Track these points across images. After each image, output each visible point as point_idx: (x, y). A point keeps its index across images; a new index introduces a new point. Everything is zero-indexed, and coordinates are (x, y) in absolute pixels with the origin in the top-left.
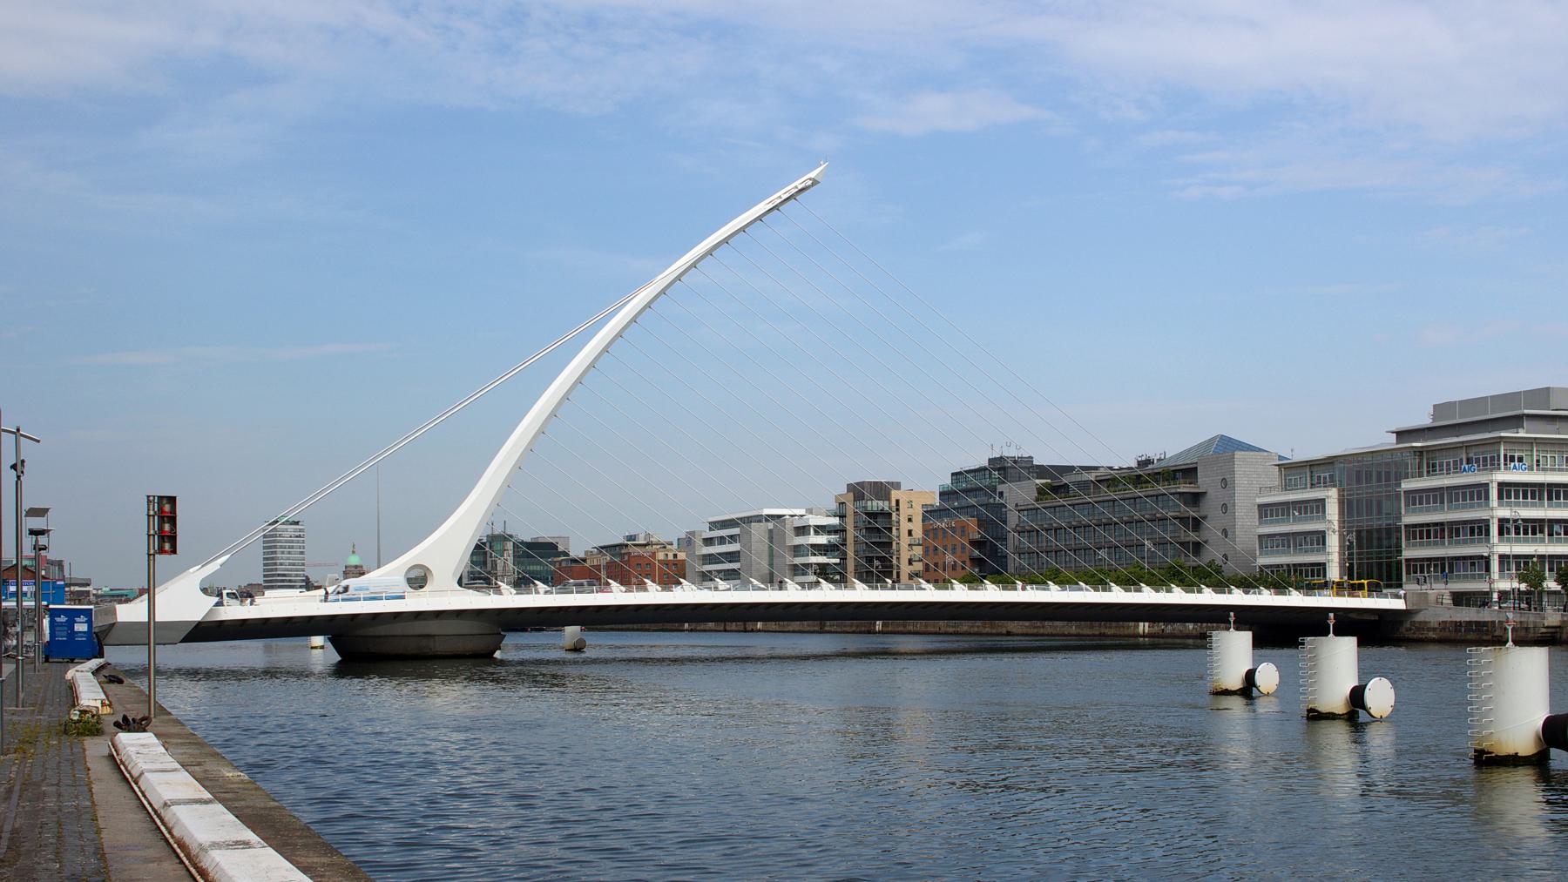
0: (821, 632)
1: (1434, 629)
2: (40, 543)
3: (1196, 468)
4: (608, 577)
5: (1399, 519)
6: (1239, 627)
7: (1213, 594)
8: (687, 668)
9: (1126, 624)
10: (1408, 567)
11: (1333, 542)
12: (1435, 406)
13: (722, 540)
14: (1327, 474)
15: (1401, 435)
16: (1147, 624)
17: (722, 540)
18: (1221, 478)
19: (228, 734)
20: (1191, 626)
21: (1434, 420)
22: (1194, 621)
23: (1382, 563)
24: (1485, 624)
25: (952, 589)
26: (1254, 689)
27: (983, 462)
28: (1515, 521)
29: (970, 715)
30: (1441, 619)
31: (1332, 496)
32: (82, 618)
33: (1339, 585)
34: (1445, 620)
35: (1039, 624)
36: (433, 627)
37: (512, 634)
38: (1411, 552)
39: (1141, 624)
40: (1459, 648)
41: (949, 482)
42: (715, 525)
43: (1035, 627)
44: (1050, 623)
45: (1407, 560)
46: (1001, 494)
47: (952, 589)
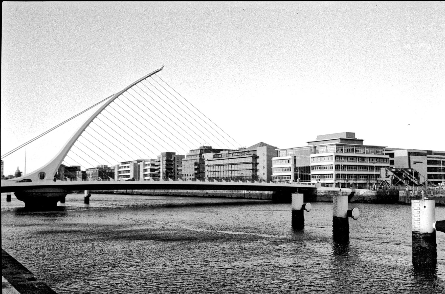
1: (323, 193)
2: (251, 161)
4: (99, 177)
5: (310, 164)
6: (300, 192)
9: (240, 191)
12: (317, 136)
13: (125, 167)
14: (372, 151)
16: (245, 191)
17: (125, 167)
18: (262, 153)
22: (172, 189)
23: (302, 176)
24: (336, 191)
25: (178, 181)
26: (304, 210)
28: (341, 165)
29: (189, 216)
30: (325, 190)
34: (325, 190)
36: (47, 190)
37: (93, 194)
38: (313, 172)
39: (244, 191)
41: (189, 153)
42: (123, 163)
45: (312, 175)
46: (203, 156)
47: (178, 181)
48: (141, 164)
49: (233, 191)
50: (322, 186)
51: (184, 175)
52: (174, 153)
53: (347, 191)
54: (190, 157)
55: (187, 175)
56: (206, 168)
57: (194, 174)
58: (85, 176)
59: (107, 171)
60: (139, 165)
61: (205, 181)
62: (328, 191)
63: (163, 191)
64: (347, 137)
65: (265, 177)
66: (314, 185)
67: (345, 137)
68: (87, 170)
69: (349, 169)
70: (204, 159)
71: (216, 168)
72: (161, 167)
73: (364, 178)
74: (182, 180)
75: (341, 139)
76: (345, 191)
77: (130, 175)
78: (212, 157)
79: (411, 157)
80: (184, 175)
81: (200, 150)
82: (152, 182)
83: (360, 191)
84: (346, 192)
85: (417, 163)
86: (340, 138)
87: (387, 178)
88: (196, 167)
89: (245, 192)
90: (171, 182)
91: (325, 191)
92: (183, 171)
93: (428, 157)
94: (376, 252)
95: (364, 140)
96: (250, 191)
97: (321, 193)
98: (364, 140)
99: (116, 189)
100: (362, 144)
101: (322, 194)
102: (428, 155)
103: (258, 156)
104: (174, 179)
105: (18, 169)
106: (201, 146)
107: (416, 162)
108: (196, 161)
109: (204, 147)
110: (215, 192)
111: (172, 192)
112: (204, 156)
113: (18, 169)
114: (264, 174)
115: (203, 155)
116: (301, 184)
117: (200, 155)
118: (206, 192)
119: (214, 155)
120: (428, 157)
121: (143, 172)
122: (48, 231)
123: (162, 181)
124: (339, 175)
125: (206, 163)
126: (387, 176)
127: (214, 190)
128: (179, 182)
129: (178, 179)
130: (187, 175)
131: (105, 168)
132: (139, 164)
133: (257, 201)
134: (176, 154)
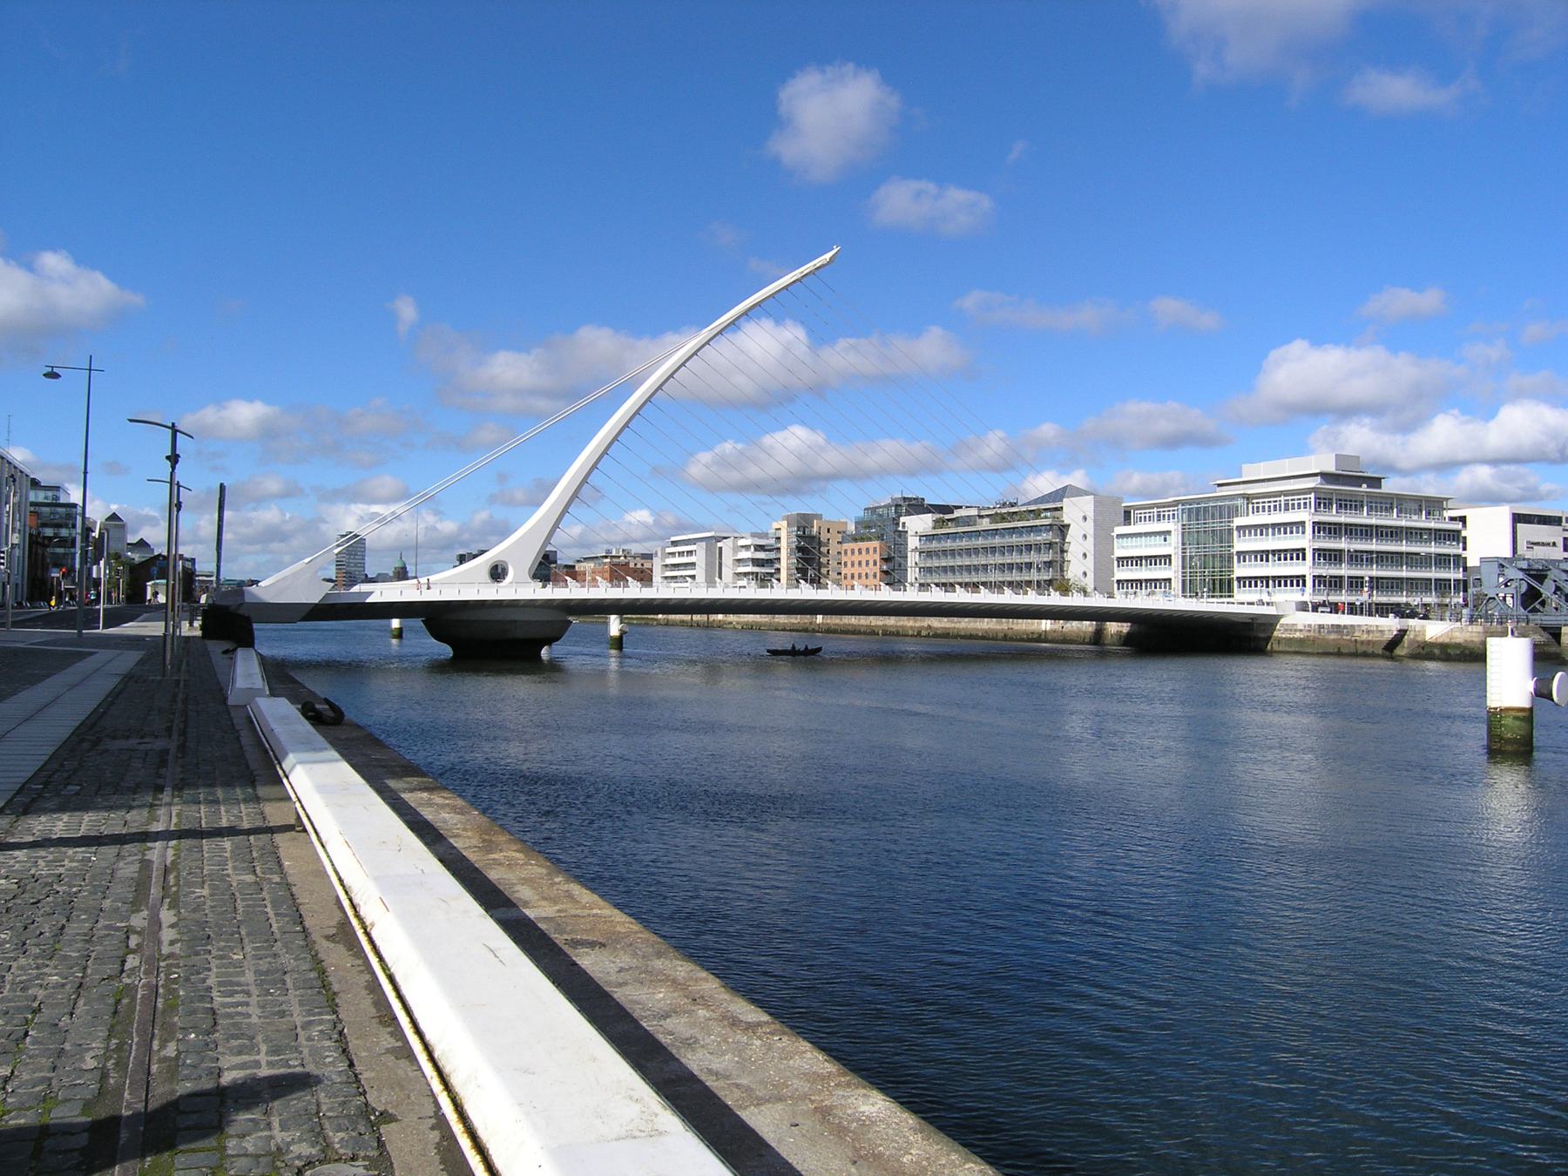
1: (1301, 630)
11: (1176, 562)
16: (1049, 621)
31: (1172, 526)
38: (1240, 570)
46: (904, 523)
50: (1298, 610)
52: (819, 517)
53: (1382, 626)
56: (1172, 547)
60: (721, 548)
61: (979, 592)
62: (1320, 625)
63: (796, 619)
64: (1337, 470)
65: (1089, 583)
66: (1274, 607)
68: (578, 561)
69: (1382, 561)
70: (907, 532)
72: (784, 555)
74: (1264, 601)
75: (1326, 476)
76: (1377, 626)
78: (931, 524)
82: (753, 592)
83: (1423, 627)
84: (1380, 629)
85: (1535, 547)
86: (1317, 471)
90: (806, 592)
91: (1310, 626)
97: (1296, 630)
99: (663, 614)
101: (1298, 635)
103: (1066, 522)
104: (816, 582)
107: (1533, 544)
112: (906, 524)
114: (1085, 574)
115: (902, 519)
116: (1228, 603)
118: (925, 624)
119: (936, 521)
121: (731, 567)
123: (779, 591)
124: (1447, 583)
129: (1048, 590)
131: (625, 557)
132: (719, 545)
133: (1045, 647)
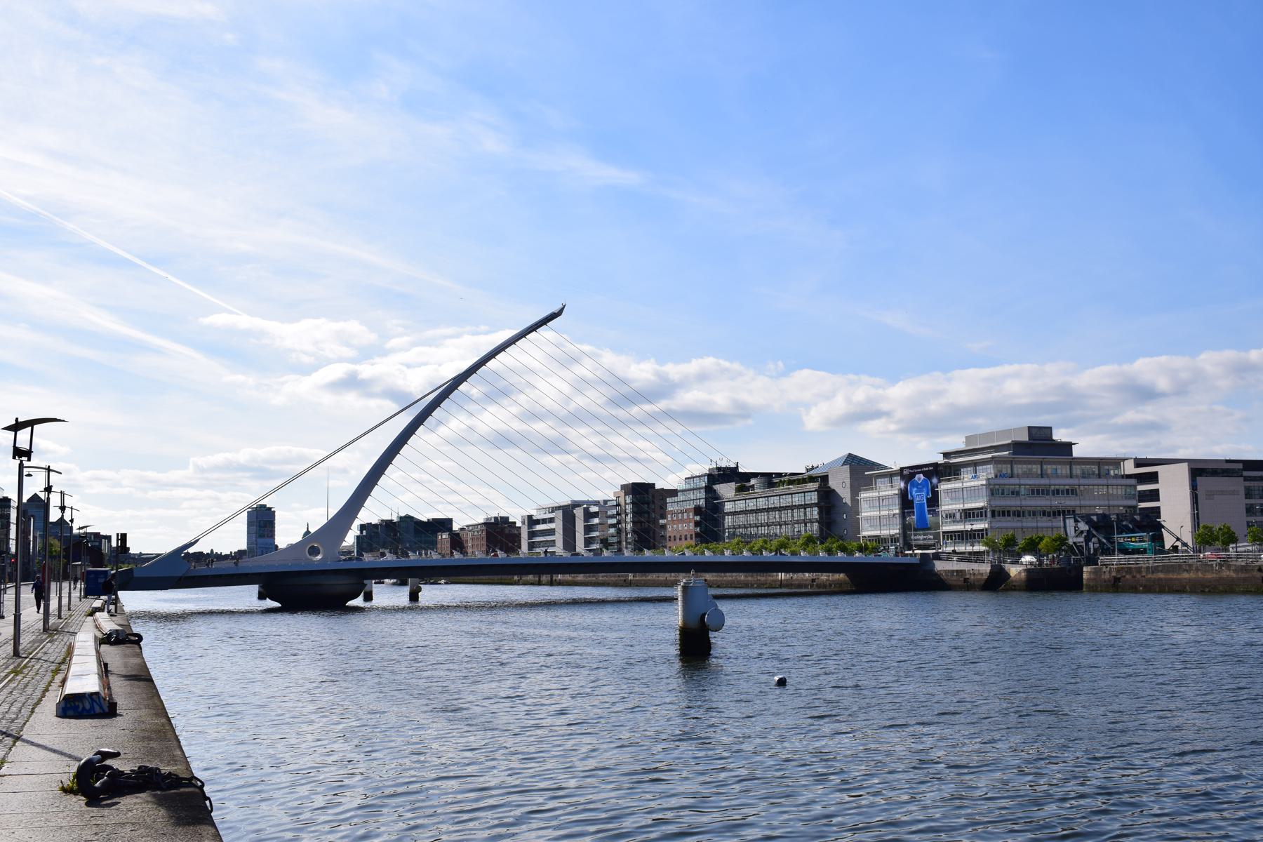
0: (539, 583)
3: (828, 476)
7: (387, 517)
8: (214, 618)
10: (944, 536)
15: (946, 455)
16: (783, 574)
19: (356, 645)
20: (807, 575)
21: (967, 445)
22: (786, 571)
24: (961, 571)
27: (320, 370)
32: (102, 576)
33: (1255, 592)
35: (723, 574)
39: (780, 574)
40: (924, 593)
43: (721, 577)
44: (730, 574)
48: (579, 513)
49: (746, 576)
51: (672, 539)
54: (686, 493)
55: (683, 539)
56: (728, 521)
57: (694, 536)
58: (457, 541)
59: (507, 531)
67: (1024, 437)
71: (812, 512)
73: (951, 539)
76: (979, 570)
77: (554, 541)
79: (1200, 480)
80: (672, 539)
81: (706, 477)
84: (981, 572)
87: (1077, 536)
88: (698, 518)
89: (782, 576)
90: (648, 555)
92: (669, 528)
93: (1246, 479)
94: (651, 663)
95: (1074, 444)
96: (791, 575)
98: (1074, 444)
100: (1072, 455)
102: (1246, 473)
105: (308, 528)
106: (711, 467)
108: (697, 502)
109: (719, 469)
110: (721, 579)
111: (564, 578)
113: (308, 528)
117: (709, 489)
120: (1246, 479)
122: (177, 621)
125: (728, 507)
126: (1078, 532)
127: (720, 574)
128: (667, 555)
130: (683, 539)
134: (657, 487)
